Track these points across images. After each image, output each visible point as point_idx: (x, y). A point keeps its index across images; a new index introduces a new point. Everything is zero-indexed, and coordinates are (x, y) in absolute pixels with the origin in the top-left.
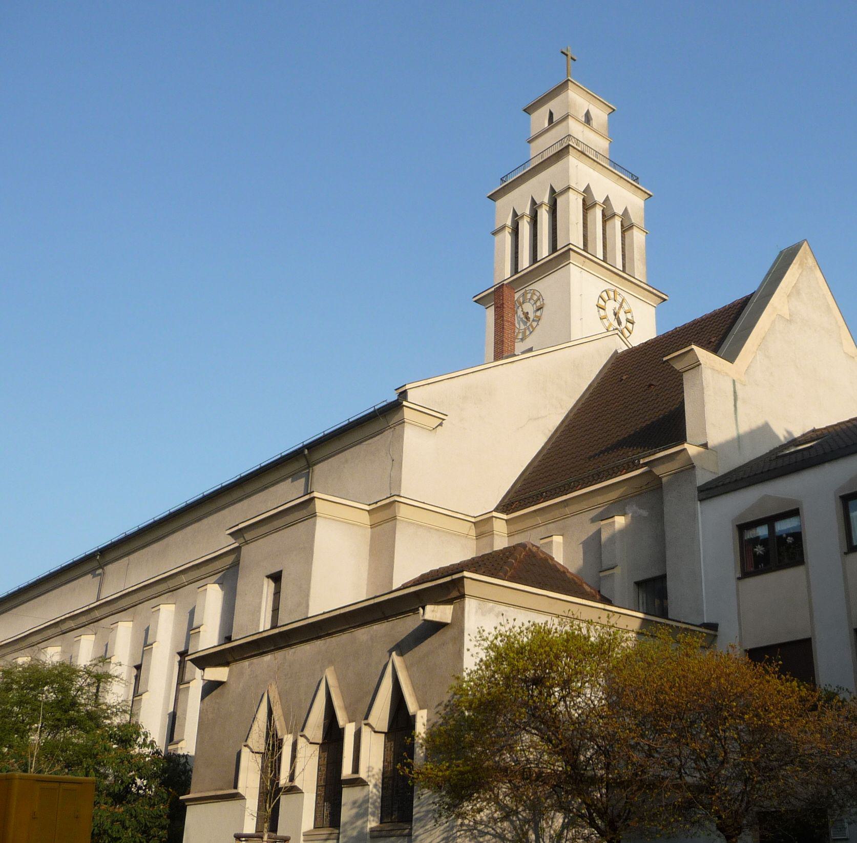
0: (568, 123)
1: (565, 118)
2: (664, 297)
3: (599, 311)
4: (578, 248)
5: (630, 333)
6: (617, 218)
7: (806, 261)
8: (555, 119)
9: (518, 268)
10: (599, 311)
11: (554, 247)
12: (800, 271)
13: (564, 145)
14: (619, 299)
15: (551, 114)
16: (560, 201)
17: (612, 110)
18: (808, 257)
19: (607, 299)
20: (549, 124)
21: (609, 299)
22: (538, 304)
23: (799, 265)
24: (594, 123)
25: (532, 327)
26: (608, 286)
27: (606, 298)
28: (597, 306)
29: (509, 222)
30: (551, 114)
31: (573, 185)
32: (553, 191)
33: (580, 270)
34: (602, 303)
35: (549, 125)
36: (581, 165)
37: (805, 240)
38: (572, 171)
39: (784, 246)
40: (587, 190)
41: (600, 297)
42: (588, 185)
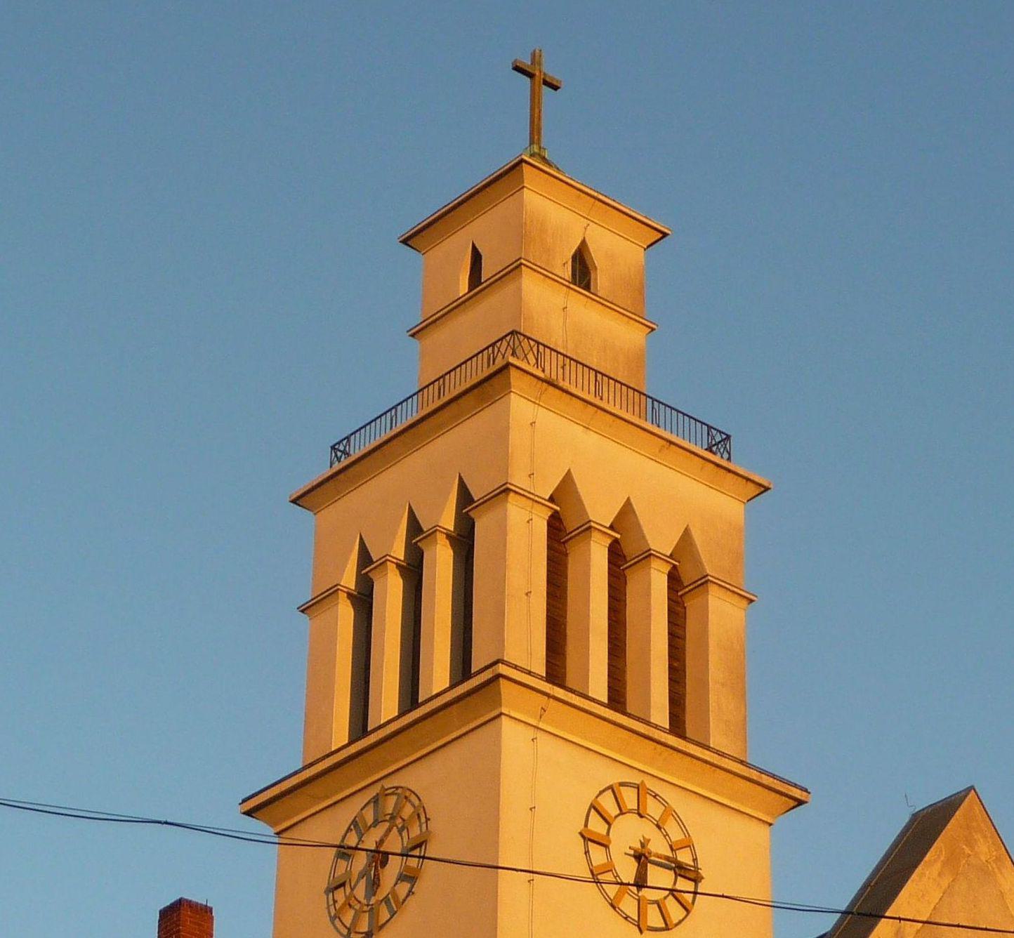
0: (520, 289)
1: (514, 270)
2: (797, 793)
3: (587, 852)
4: (530, 673)
5: (688, 911)
6: (655, 564)
7: (967, 851)
8: (487, 272)
9: (367, 725)
10: (587, 852)
11: (462, 665)
12: (945, 882)
13: (499, 363)
14: (654, 809)
15: (476, 257)
16: (483, 526)
17: (661, 235)
18: (978, 836)
19: (616, 811)
20: (471, 287)
21: (622, 813)
22: (415, 831)
23: (945, 864)
24: (601, 280)
25: (395, 896)
26: (615, 775)
27: (612, 810)
28: (581, 834)
29: (349, 580)
30: (476, 257)
31: (518, 479)
32: (465, 497)
33: (531, 733)
34: (597, 826)
35: (470, 290)
36: (545, 417)
37: (972, 788)
38: (518, 438)
39: (926, 798)
40: (565, 492)
41: (593, 807)
42: (569, 473)
